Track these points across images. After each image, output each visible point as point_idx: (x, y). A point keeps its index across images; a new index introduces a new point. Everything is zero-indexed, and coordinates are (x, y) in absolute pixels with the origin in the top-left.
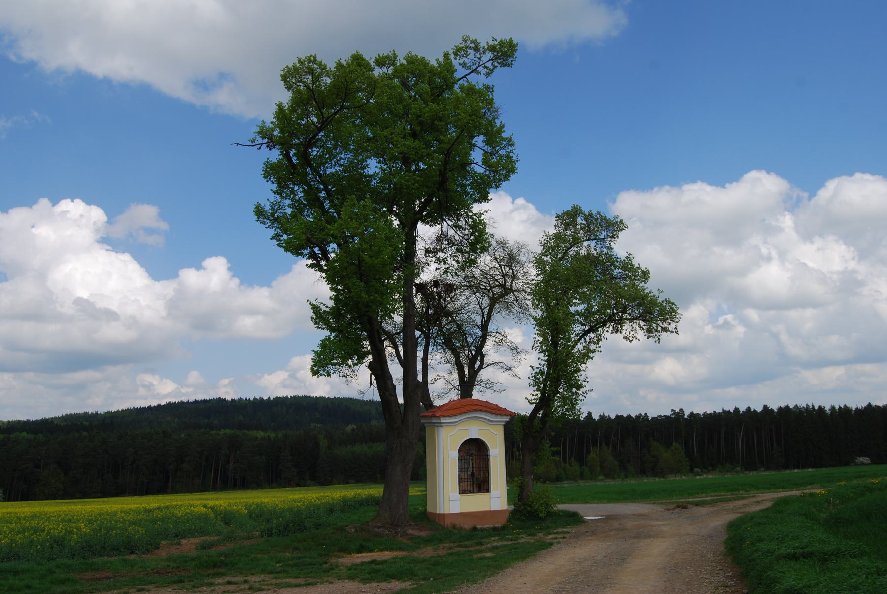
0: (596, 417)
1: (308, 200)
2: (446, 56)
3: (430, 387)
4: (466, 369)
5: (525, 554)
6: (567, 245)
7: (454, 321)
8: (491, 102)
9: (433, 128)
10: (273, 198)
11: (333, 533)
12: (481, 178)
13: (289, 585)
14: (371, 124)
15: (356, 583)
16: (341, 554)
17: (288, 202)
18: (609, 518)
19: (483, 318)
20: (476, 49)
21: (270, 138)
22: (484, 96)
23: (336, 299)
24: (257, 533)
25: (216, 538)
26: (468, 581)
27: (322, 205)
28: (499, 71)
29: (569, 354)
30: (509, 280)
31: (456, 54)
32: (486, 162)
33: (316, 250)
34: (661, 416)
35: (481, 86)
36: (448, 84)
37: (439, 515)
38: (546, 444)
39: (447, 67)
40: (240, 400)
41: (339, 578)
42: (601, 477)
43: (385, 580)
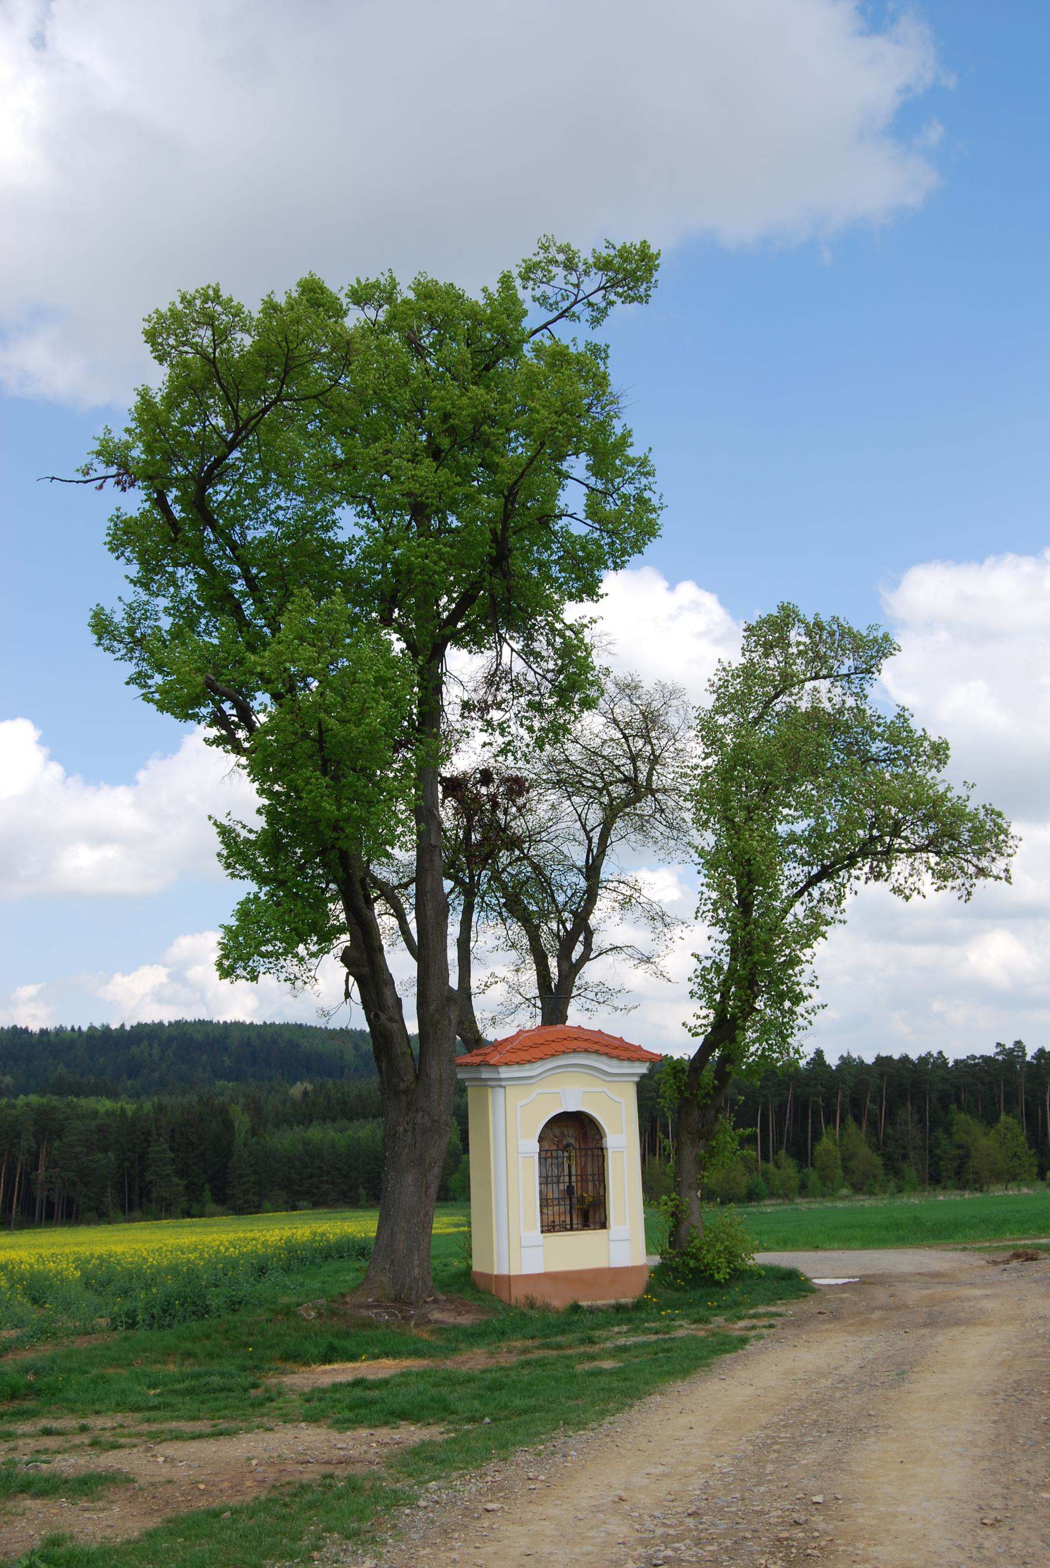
0: (832, 1060)
1: (209, 601)
2: (506, 281)
3: (475, 1001)
4: (553, 963)
5: (687, 1362)
6: (770, 689)
7: (526, 857)
8: (601, 382)
9: (477, 439)
10: (134, 594)
11: (269, 1320)
12: (583, 548)
13: (177, 1437)
14: (345, 434)
15: (323, 1430)
16: (289, 1366)
17: (162, 602)
18: (867, 1281)
19: (590, 850)
20: (570, 265)
21: (124, 466)
22: (587, 370)
23: (269, 812)
24: (103, 1322)
25: (14, 1333)
26: (567, 1423)
27: (237, 610)
28: (622, 311)
29: (775, 929)
30: (644, 767)
31: (525, 278)
32: (593, 512)
33: (227, 706)
34: (973, 1057)
35: (581, 348)
36: (509, 345)
37: (499, 1278)
38: (726, 1121)
39: (508, 306)
40: (60, 1030)
41: (286, 1419)
42: (845, 1191)
43: (386, 1423)
